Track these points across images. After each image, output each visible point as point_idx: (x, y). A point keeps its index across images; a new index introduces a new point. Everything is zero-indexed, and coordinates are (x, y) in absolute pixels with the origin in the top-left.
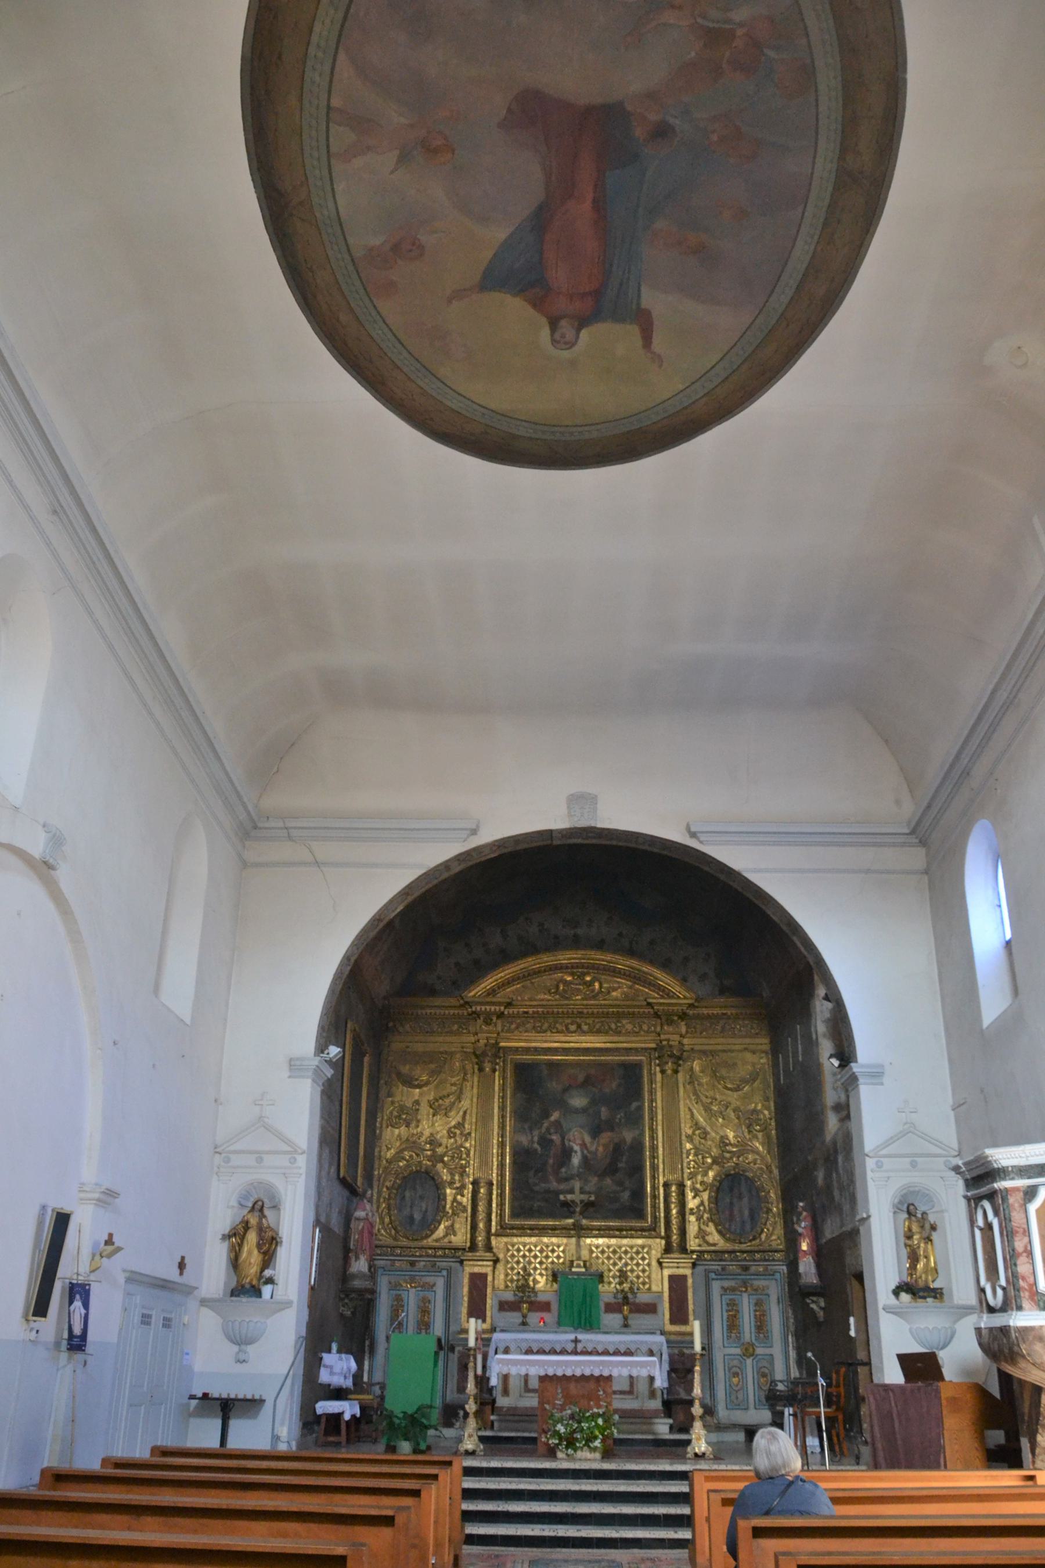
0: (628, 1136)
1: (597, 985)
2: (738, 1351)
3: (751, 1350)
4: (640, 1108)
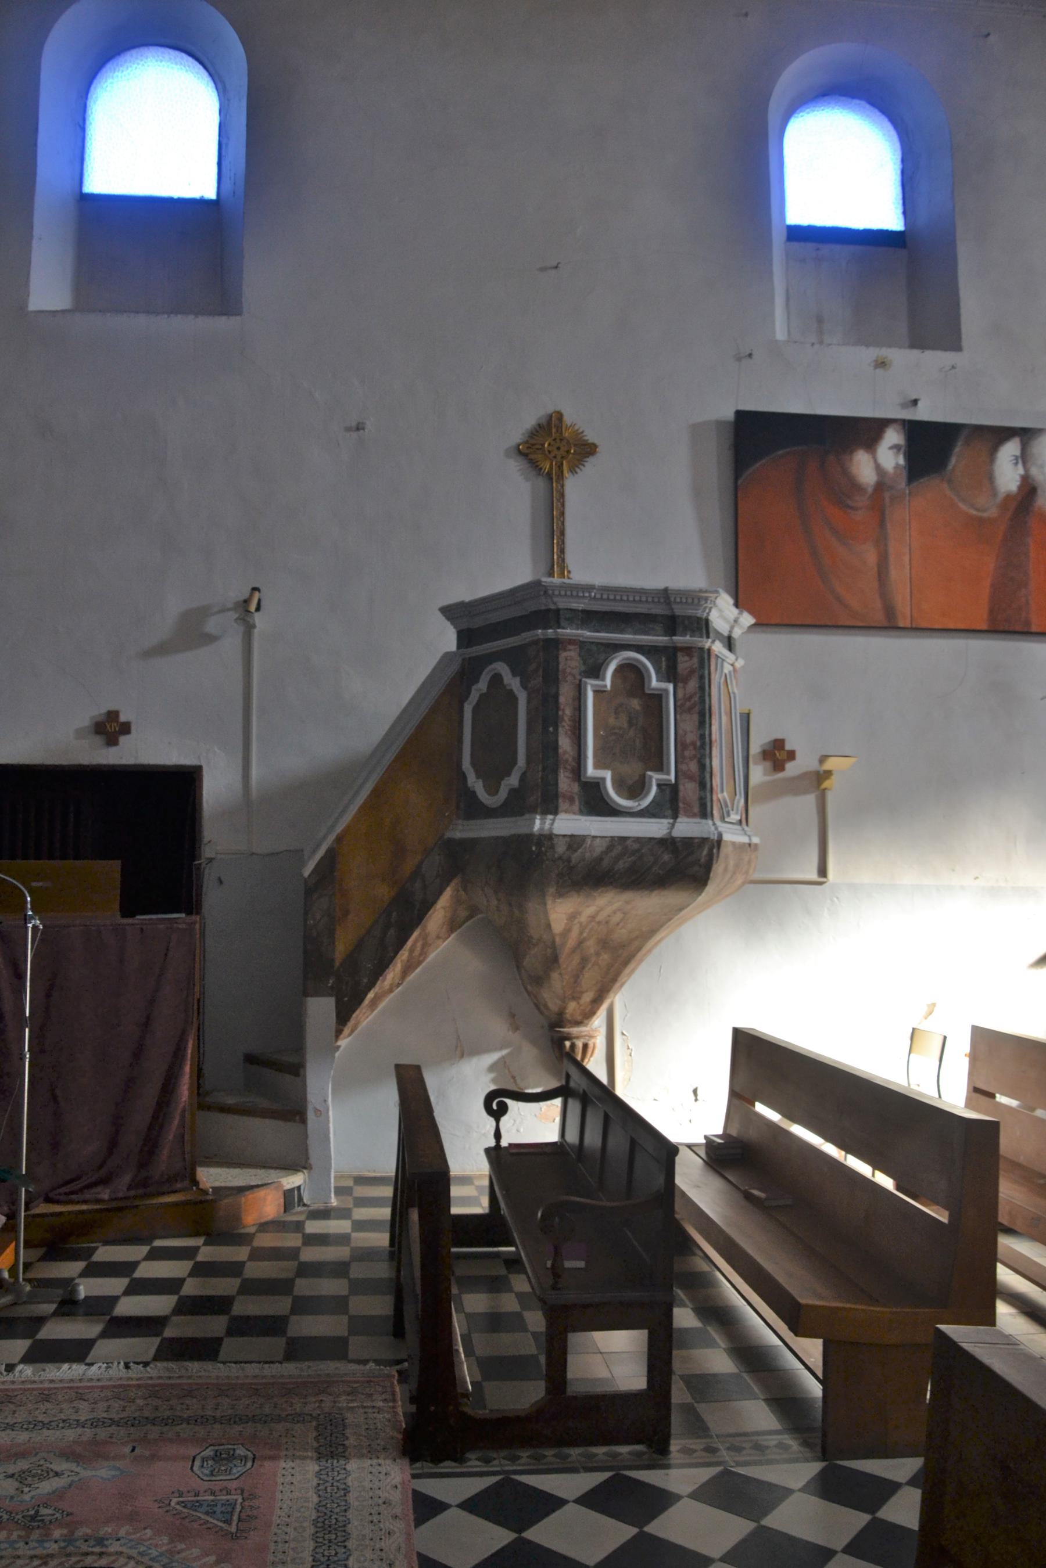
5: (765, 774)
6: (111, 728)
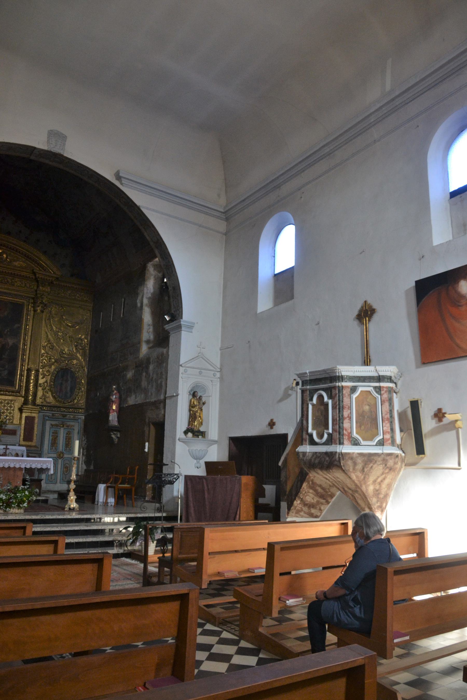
0: (11, 342)
1: (5, 256)
2: (55, 455)
3: (62, 455)
4: (20, 328)
5: (436, 423)
6: (272, 424)
